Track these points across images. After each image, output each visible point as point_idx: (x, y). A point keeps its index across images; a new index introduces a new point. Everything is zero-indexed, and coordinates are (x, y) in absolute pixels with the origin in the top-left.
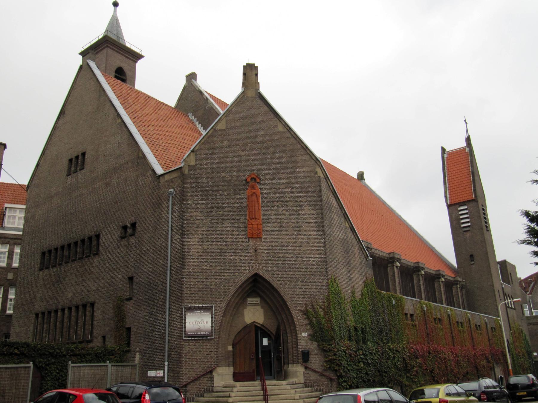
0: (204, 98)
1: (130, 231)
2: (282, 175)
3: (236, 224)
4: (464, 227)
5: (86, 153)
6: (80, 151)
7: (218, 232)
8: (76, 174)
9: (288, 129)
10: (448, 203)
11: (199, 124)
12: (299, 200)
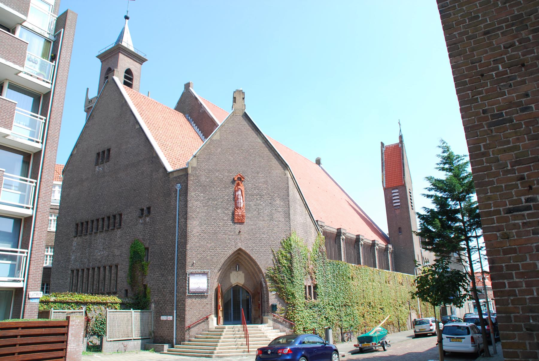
0: (198, 103)
1: (145, 212)
2: (260, 175)
3: (226, 212)
4: (395, 206)
5: (111, 150)
6: (105, 147)
7: (213, 217)
8: (103, 165)
9: (266, 140)
10: (385, 187)
11: (194, 123)
12: (272, 195)
